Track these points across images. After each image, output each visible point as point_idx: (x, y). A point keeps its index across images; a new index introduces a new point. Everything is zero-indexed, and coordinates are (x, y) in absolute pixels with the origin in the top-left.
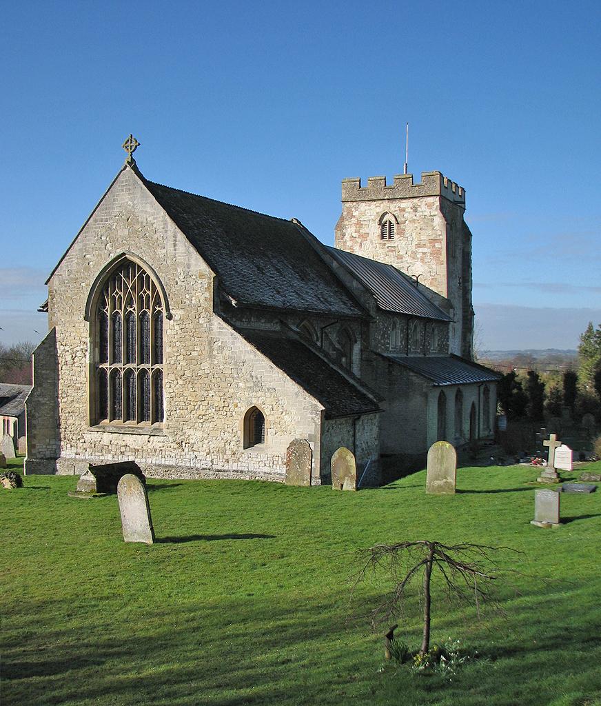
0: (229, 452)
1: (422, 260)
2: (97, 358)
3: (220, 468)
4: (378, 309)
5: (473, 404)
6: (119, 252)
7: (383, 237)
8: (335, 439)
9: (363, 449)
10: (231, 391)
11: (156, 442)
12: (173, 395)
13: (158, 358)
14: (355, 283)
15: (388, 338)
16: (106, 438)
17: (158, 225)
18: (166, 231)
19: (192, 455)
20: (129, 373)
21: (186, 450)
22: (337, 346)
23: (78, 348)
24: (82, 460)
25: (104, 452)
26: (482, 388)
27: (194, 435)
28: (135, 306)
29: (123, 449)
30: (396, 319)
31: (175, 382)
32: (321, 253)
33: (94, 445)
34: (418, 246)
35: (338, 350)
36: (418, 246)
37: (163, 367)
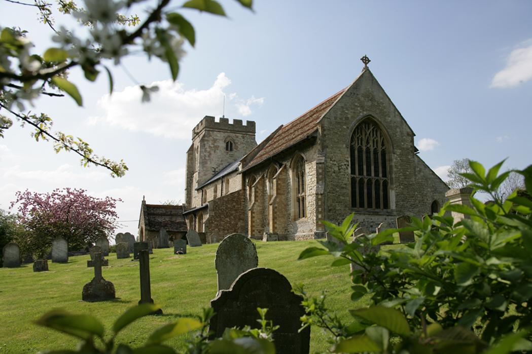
7: (227, 149)
10: (425, 192)
29: (372, 224)
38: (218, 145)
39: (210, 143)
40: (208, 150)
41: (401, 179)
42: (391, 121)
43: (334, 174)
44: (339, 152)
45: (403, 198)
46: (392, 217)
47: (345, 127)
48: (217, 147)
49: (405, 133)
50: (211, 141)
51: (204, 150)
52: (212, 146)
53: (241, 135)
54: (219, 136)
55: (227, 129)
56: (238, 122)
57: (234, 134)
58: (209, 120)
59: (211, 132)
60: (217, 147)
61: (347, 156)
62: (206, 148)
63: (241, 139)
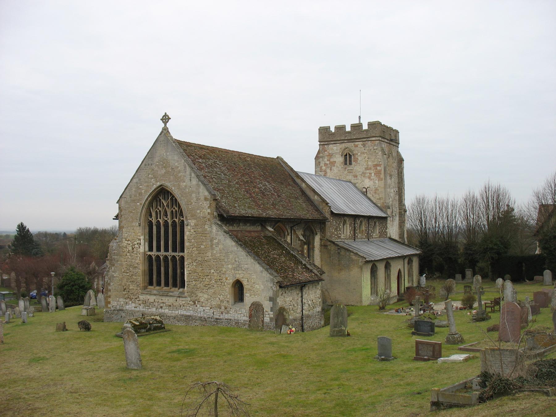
0: (223, 308)
1: (369, 178)
2: (147, 249)
3: (218, 317)
4: (332, 213)
5: (400, 271)
6: (159, 184)
7: (346, 164)
8: (288, 299)
9: (309, 305)
10: (224, 270)
11: (181, 301)
12: (190, 272)
13: (182, 250)
14: (316, 197)
15: (340, 230)
16: (152, 298)
17: (181, 168)
18: (186, 172)
19: (201, 309)
20: (166, 257)
21: (198, 306)
22: (302, 238)
23: (136, 243)
24: (138, 311)
25: (151, 306)
26: (406, 261)
27: (203, 297)
28: (169, 217)
29: (162, 305)
30: (346, 218)
31: (192, 264)
32: (295, 178)
33: (145, 302)
34: (367, 169)
35: (302, 240)
36: (367, 169)
37: (186, 254)
38: (335, 160)
39: (326, 160)
40: (324, 168)
41: (194, 255)
42: (186, 186)
43: (128, 254)
44: (132, 231)
45: (195, 277)
46: (184, 299)
47: (138, 204)
48: (333, 163)
49: (202, 198)
50: (326, 157)
51: (319, 169)
52: (328, 162)
53: (361, 143)
54: (336, 149)
55: (343, 138)
56: (340, 129)
57: (353, 144)
58: (324, 132)
59: (326, 146)
60: (333, 163)
61: (139, 234)
62: (322, 167)
63: (361, 147)
